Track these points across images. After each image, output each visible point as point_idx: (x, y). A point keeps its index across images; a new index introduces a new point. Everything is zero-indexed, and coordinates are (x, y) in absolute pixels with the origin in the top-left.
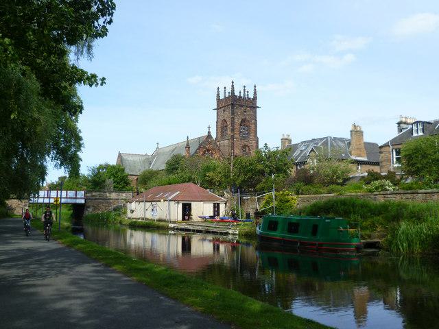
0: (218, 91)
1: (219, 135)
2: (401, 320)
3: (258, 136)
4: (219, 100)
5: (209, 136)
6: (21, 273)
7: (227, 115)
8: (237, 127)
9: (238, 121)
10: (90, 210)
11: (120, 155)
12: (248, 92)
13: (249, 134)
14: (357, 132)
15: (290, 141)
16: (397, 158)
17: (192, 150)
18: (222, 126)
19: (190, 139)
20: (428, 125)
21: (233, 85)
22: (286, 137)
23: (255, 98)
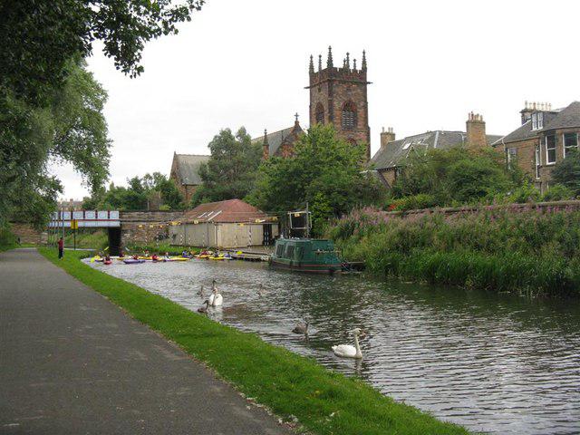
0: (312, 61)
3: (370, 125)
4: (312, 74)
5: (297, 127)
6: (276, 317)
7: (323, 97)
8: (337, 113)
9: (338, 104)
10: (128, 235)
11: (176, 157)
12: (355, 60)
13: (355, 122)
14: (476, 123)
15: (393, 136)
16: (567, 150)
18: (317, 113)
19: (268, 133)
20: (550, 116)
21: (330, 53)
22: (386, 130)
23: (364, 69)
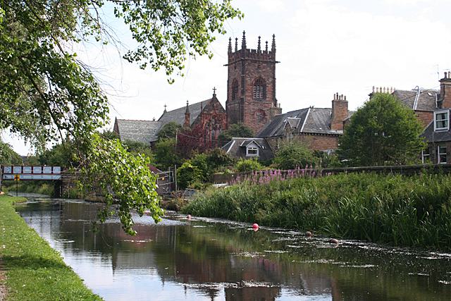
1: (231, 98)
2: (21, 155)
4: (230, 54)
5: (214, 99)
13: (264, 96)
17: (193, 118)
23: (274, 50)
